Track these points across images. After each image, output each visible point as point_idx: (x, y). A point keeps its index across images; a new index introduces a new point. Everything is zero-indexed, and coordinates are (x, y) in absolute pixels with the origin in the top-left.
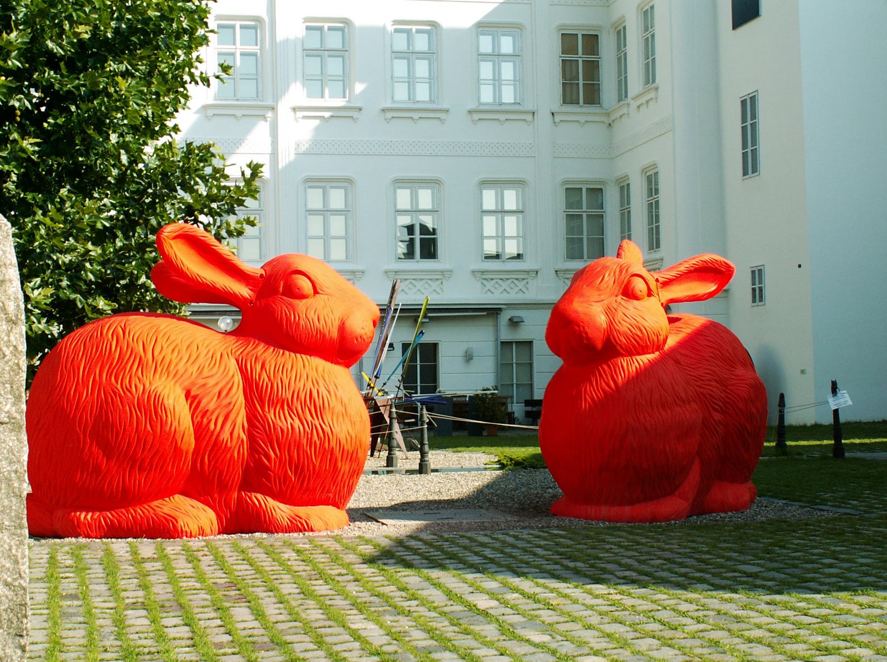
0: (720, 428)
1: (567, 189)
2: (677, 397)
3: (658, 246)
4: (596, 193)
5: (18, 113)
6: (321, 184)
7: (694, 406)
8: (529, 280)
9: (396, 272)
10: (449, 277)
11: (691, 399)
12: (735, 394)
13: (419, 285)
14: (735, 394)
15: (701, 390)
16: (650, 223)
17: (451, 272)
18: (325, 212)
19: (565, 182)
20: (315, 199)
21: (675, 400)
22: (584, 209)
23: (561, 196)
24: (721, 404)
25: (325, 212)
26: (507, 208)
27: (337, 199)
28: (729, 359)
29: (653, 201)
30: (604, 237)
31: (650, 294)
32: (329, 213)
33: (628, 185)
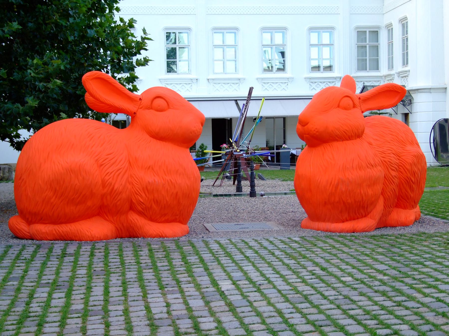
0: (395, 180)
1: (358, 32)
2: (369, 164)
3: (407, 63)
4: (375, 33)
5: (15, 6)
6: (222, 31)
7: (379, 168)
8: (336, 82)
9: (262, 79)
10: (291, 82)
11: (377, 164)
12: (405, 160)
13: (275, 86)
14: (405, 160)
15: (385, 159)
16: (403, 50)
17: (293, 78)
18: (223, 46)
19: (357, 28)
20: (218, 39)
21: (367, 165)
22: (368, 42)
23: (354, 35)
24: (396, 166)
25: (223, 46)
26: (324, 42)
27: (230, 39)
28: (403, 141)
29: (405, 38)
30: (379, 58)
31: (354, 106)
32: (225, 47)
33: (392, 29)
